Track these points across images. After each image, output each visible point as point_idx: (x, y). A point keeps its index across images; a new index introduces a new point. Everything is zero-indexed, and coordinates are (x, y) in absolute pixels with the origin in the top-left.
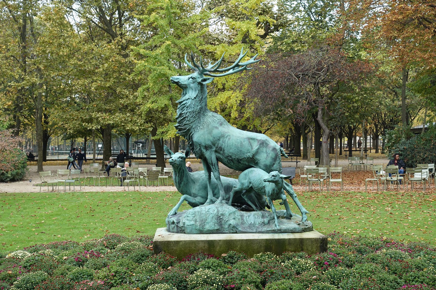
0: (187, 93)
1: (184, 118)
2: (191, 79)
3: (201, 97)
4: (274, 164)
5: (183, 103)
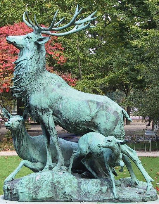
0: (24, 53)
1: (20, 80)
2: (27, 39)
3: (38, 58)
4: (114, 128)
5: (20, 64)
